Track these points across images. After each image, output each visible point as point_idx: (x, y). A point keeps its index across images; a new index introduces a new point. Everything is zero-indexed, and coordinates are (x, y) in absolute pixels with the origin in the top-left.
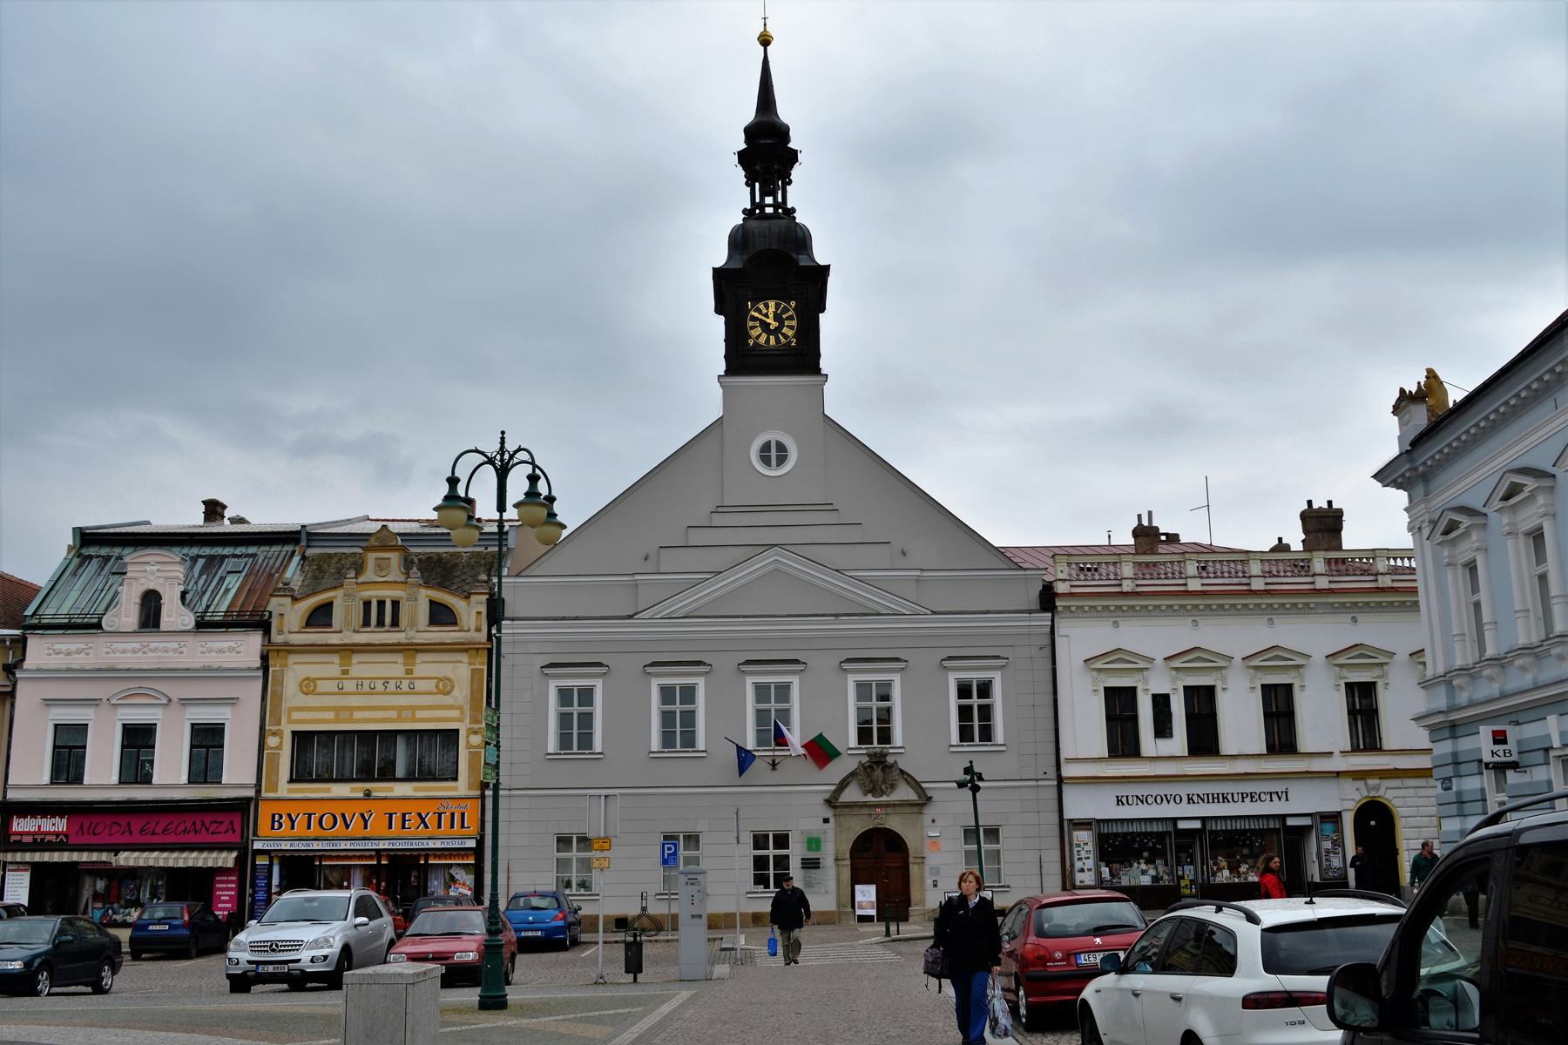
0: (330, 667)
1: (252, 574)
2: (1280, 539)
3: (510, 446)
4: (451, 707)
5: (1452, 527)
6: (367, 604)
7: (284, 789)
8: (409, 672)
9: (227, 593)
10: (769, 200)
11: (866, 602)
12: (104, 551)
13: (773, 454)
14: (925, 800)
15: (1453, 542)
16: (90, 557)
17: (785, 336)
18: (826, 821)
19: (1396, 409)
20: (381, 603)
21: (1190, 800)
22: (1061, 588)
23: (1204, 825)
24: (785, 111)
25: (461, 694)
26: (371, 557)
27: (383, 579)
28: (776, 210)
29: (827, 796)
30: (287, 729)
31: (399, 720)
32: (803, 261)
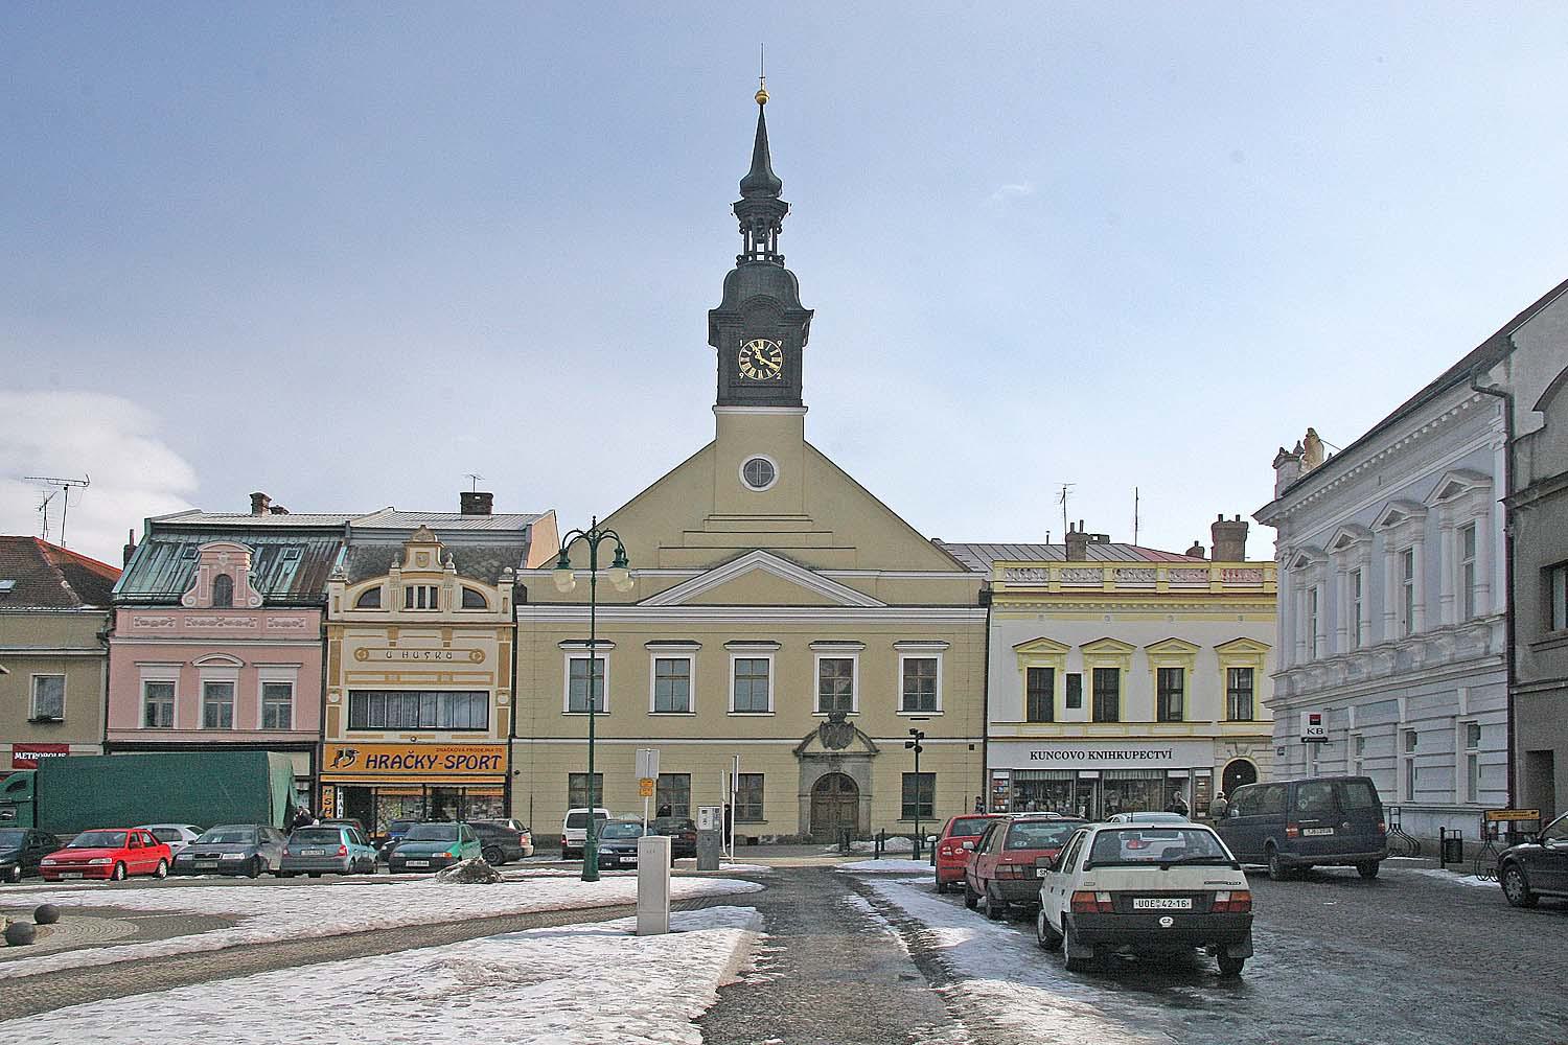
0: (381, 638)
1: (306, 559)
2: (1197, 543)
6: (410, 589)
7: (344, 735)
10: (760, 248)
12: (173, 539)
16: (161, 544)
17: (772, 371)
19: (1276, 465)
20: (422, 589)
22: (997, 588)
23: (1101, 775)
24: (778, 167)
25: (492, 663)
26: (412, 551)
28: (767, 257)
29: (796, 747)
31: (439, 682)
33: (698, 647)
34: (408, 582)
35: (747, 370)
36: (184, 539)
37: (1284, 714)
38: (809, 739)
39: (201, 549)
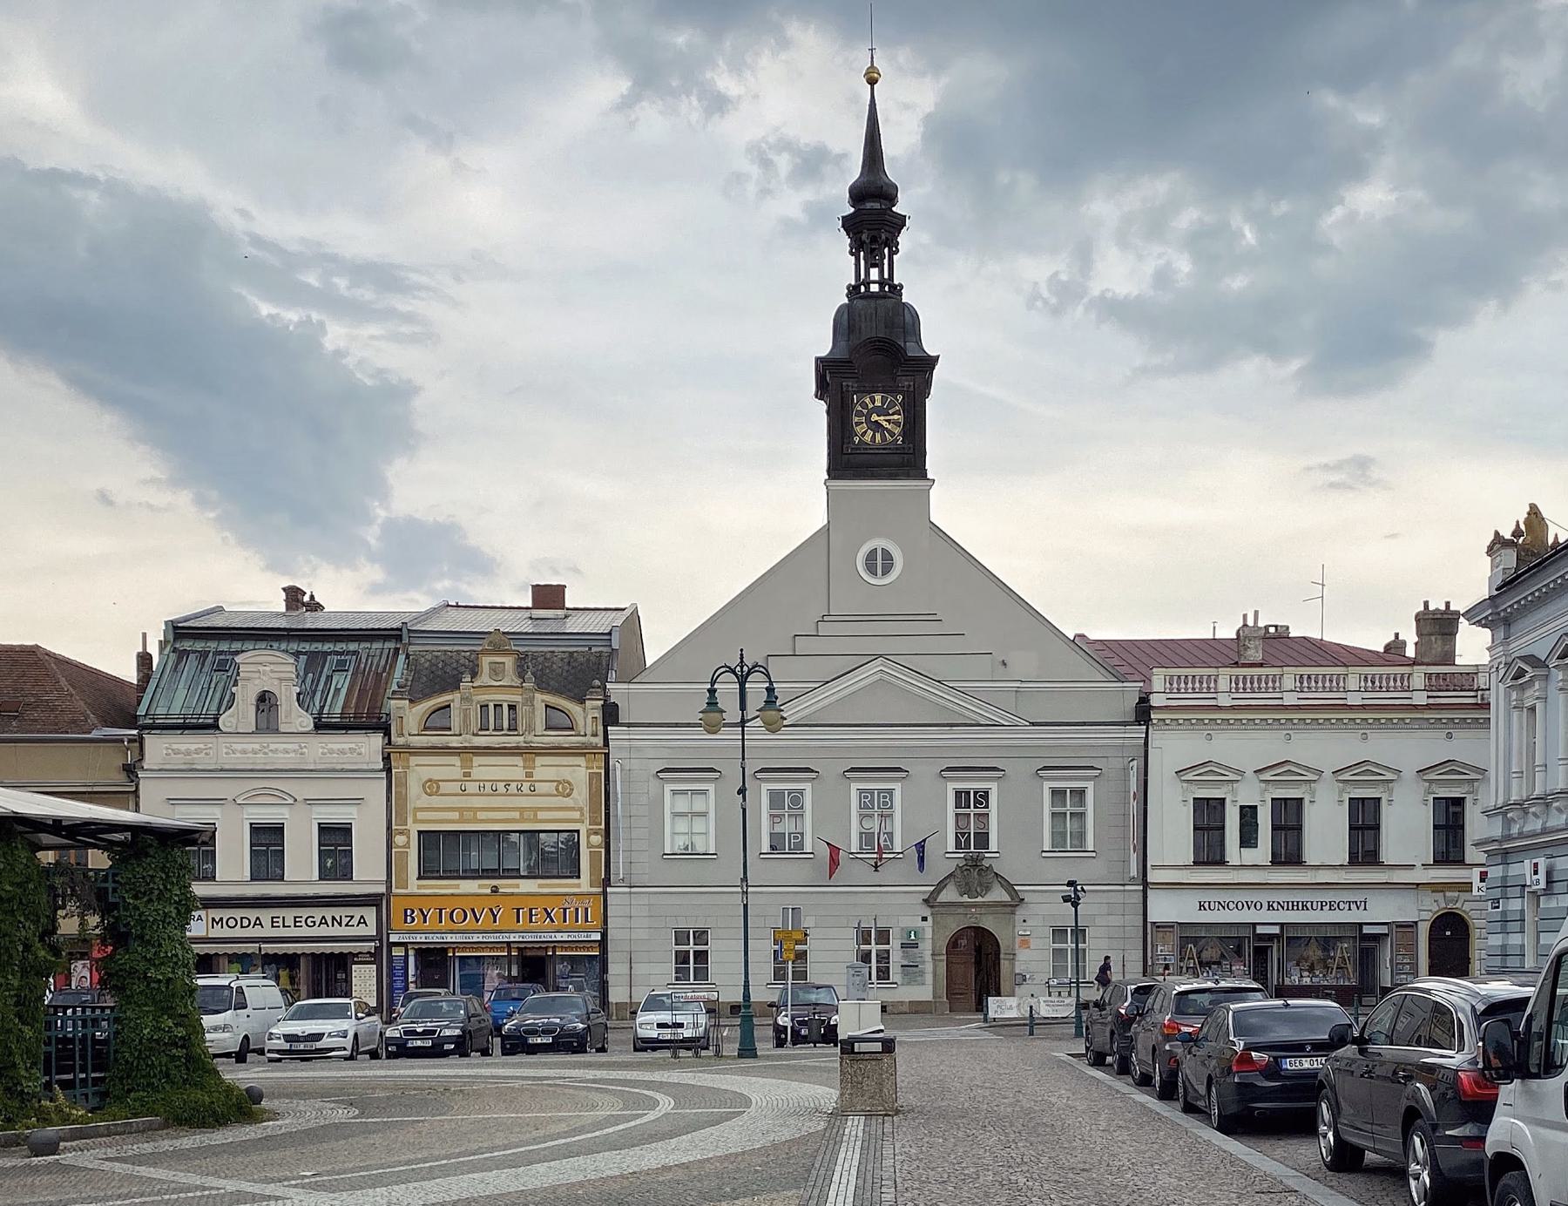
0: (448, 769)
2: (1397, 635)
3: (749, 662)
4: (572, 809)
5: (1521, 673)
7: (414, 885)
8: (529, 775)
9: (339, 693)
10: (874, 274)
11: (967, 713)
12: (199, 646)
13: (879, 562)
14: (1017, 901)
15: (1523, 688)
16: (186, 653)
17: (892, 434)
18: (924, 919)
19: (1490, 551)
21: (1270, 906)
24: (892, 172)
25: (581, 796)
26: (486, 661)
27: (497, 682)
30: (414, 829)
32: (912, 352)
33: (813, 775)
34: (483, 698)
35: (864, 434)
36: (212, 645)
37: (1499, 859)
38: (941, 886)
39: (238, 659)
